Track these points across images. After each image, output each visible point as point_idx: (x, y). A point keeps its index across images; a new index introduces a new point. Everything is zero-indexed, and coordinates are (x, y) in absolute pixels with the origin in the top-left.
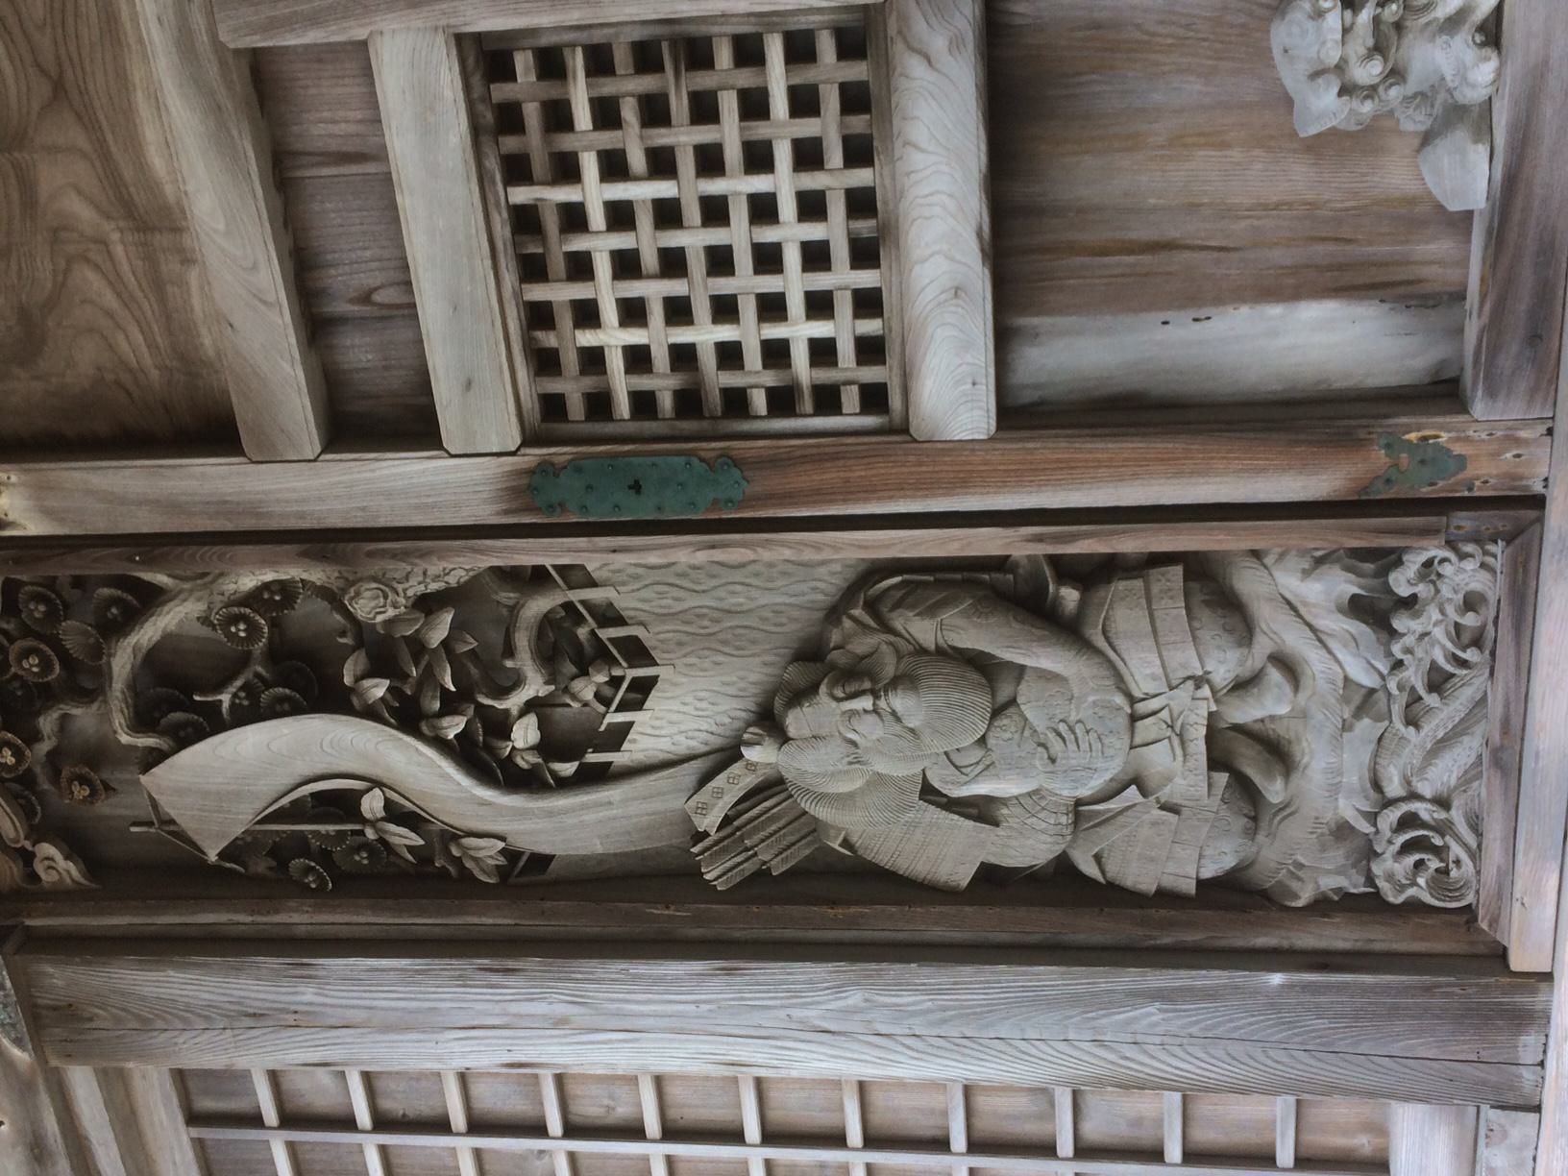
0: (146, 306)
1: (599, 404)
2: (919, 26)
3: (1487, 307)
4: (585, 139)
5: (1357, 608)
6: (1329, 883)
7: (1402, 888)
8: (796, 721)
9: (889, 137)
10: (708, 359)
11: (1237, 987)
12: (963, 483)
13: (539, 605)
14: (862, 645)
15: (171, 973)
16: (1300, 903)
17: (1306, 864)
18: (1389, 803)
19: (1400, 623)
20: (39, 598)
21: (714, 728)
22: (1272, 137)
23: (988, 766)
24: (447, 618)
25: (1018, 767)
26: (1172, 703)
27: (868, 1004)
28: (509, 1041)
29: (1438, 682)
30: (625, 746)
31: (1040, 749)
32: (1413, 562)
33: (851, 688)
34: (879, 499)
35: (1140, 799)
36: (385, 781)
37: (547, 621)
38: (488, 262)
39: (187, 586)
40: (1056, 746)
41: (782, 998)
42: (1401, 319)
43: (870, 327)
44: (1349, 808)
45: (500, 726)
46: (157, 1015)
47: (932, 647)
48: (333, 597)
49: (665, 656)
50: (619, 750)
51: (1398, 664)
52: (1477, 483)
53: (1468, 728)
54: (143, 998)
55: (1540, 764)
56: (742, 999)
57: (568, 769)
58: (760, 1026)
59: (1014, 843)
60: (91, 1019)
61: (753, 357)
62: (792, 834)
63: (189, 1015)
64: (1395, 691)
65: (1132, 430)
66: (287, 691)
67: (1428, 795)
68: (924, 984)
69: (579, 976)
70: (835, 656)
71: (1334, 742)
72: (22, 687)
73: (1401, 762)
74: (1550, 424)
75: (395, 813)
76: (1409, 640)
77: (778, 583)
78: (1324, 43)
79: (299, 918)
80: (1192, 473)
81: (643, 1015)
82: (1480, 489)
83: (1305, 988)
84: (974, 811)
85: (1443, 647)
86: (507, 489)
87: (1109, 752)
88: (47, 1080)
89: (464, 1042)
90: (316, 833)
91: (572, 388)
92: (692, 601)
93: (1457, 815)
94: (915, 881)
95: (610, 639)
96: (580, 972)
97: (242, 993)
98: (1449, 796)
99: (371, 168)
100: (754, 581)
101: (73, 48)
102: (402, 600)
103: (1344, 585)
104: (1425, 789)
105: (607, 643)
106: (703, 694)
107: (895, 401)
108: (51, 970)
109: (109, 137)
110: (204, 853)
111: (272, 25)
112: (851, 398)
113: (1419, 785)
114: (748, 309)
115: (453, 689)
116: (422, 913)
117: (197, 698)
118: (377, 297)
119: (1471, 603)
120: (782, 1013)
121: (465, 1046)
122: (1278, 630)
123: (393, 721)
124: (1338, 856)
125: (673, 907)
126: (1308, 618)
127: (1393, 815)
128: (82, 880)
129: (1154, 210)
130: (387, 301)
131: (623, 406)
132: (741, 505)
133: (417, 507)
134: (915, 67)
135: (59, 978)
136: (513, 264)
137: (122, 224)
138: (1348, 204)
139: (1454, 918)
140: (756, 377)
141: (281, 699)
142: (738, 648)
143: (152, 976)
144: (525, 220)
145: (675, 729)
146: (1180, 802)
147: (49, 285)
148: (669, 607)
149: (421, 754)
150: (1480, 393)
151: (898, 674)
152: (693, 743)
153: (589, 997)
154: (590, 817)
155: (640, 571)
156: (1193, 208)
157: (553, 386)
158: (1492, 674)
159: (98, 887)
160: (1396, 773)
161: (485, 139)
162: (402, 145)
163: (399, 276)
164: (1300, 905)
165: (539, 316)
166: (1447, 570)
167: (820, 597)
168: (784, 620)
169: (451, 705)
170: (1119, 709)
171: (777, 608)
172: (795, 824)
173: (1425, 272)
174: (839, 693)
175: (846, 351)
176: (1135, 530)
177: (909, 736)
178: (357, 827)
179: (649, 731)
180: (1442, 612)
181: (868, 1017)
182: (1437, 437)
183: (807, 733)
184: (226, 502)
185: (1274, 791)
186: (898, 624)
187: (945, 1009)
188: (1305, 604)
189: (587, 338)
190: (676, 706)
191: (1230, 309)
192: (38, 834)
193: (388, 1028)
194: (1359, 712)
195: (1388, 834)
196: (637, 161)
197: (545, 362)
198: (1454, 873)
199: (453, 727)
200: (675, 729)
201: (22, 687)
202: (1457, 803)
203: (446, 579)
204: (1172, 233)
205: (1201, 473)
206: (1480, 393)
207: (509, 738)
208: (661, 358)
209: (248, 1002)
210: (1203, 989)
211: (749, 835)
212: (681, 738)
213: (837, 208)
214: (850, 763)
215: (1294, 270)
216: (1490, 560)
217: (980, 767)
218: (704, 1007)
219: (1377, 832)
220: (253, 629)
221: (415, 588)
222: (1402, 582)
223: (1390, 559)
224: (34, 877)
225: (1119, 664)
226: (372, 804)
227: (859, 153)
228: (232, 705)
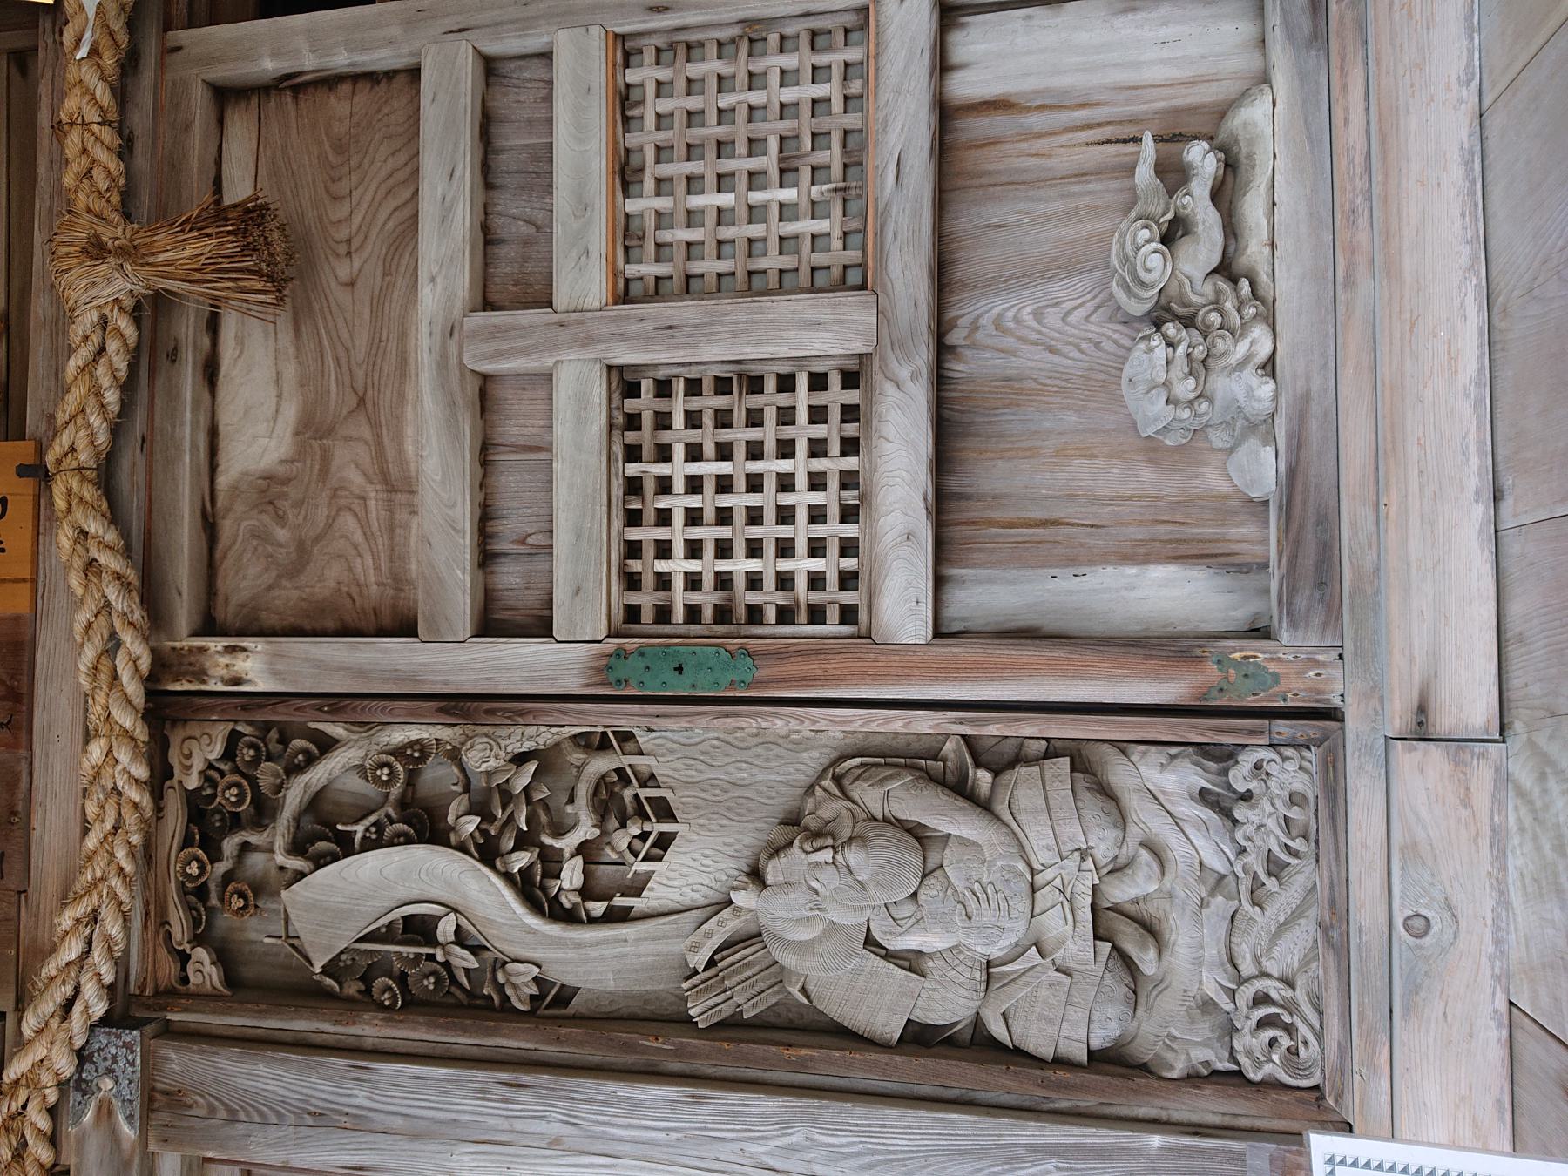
0: (380, 541)
1: (663, 614)
2: (893, 363)
3: (1284, 561)
4: (678, 437)
5: (1204, 796)
6: (1200, 1055)
7: (1258, 1064)
8: (774, 871)
9: (869, 438)
10: (740, 583)
11: (1123, 1148)
12: (906, 676)
13: (602, 764)
14: (827, 812)
15: (261, 1066)
16: (1174, 1075)
17: (1179, 1036)
18: (1242, 980)
19: (1240, 812)
20: (251, 746)
21: (713, 884)
22: (1125, 452)
23: (918, 921)
24: (532, 767)
25: (946, 925)
26: (1063, 872)
27: (808, 1143)
28: (509, 1159)
29: (1275, 867)
30: (645, 893)
31: (960, 906)
32: (1247, 760)
33: (817, 844)
34: (847, 686)
35: (1039, 960)
36: (460, 908)
37: (602, 780)
38: (605, 509)
39: (355, 737)
40: (972, 903)
41: (739, 1131)
42: (1226, 581)
43: (849, 563)
44: (1212, 983)
45: (551, 862)
46: (242, 1107)
47: (880, 817)
48: (455, 756)
49: (685, 816)
50: (639, 896)
51: (1242, 851)
52: (1290, 695)
53: (1303, 912)
54: (235, 1089)
55: (1364, 938)
56: (705, 1129)
57: (598, 908)
58: (718, 1160)
59: (937, 996)
60: (190, 1107)
61: (769, 582)
62: (763, 980)
63: (265, 1109)
64: (1241, 875)
65: (1029, 641)
66: (406, 827)
67: (1276, 974)
68: (857, 1125)
69: (576, 1096)
70: (807, 820)
71: (1195, 917)
72: (220, 820)
73: (1251, 940)
74: (1340, 651)
75: (460, 937)
76: (1249, 829)
77: (773, 764)
78: (1154, 368)
79: (369, 1029)
80: (1073, 677)
81: (622, 1140)
82: (1292, 700)
83: (1181, 1151)
84: (907, 964)
85: (1277, 837)
86: (592, 668)
87: (1014, 914)
88: (142, 1160)
89: (474, 1156)
90: (399, 954)
91: (646, 599)
92: (709, 774)
93: (1301, 996)
94: (857, 1034)
95: (646, 798)
96: (578, 1092)
97: (310, 1092)
98: (1293, 978)
99: (542, 456)
100: (756, 762)
101: (376, 378)
102: (502, 754)
103: (1192, 776)
104: (1272, 967)
105: (644, 801)
106: (708, 852)
107: (863, 616)
108: (173, 1056)
109: (385, 432)
110: (312, 965)
111: (498, 355)
112: (833, 614)
113: (1268, 964)
114: (770, 549)
115: (525, 829)
116: (465, 1031)
117: (339, 827)
118: (530, 541)
119: (1294, 799)
120: (737, 1146)
121: (474, 1160)
122: (1147, 819)
123: (476, 854)
124: (1205, 1029)
125: (661, 1040)
126: (1168, 806)
127: (1247, 992)
128: (218, 985)
129: (1046, 498)
130: (536, 543)
131: (679, 614)
132: (749, 687)
133: (526, 679)
134: (889, 388)
135: (179, 1062)
136: (621, 514)
137: (379, 487)
138: (1181, 498)
139: (1304, 1094)
140: (770, 598)
141: (398, 834)
142: (738, 814)
143: (244, 1068)
144: (633, 486)
145: (682, 882)
146: (1072, 965)
147: (322, 525)
148: (692, 777)
149: (492, 884)
150: (1284, 625)
151: (855, 834)
152: (696, 896)
153: (583, 1119)
154: (608, 951)
155: (675, 746)
156: (1072, 497)
157: (634, 598)
158: (1317, 861)
159: (229, 993)
160: (1247, 950)
161: (616, 433)
162: (562, 433)
163: (546, 526)
164: (1175, 1076)
165: (633, 549)
166: (1273, 769)
167: (802, 777)
168: (774, 794)
169: (522, 842)
170: (1022, 875)
171: (769, 784)
172: (767, 972)
173: (1236, 547)
174: (808, 847)
175: (832, 580)
176: (1031, 719)
177: (858, 887)
178: (431, 951)
179: (665, 881)
180: (1273, 805)
181: (809, 1156)
182: (1256, 657)
183: (781, 879)
184: (396, 670)
185: (1147, 961)
186: (855, 795)
187: (873, 1152)
188: (1164, 793)
189: (662, 566)
190: (686, 860)
191: (1100, 568)
192: (198, 940)
193: (416, 1136)
194: (1213, 892)
195: (1245, 1011)
196: (709, 449)
197: (632, 582)
198: (1302, 1053)
199: (520, 860)
200: (682, 882)
201: (220, 820)
202: (1300, 982)
203: (537, 739)
204: (1057, 514)
205: (1081, 677)
206: (1284, 625)
207: (558, 877)
208: (708, 581)
209: (313, 1101)
210: (1093, 1148)
211: (730, 976)
212: (687, 890)
213: (833, 483)
214: (811, 909)
215: (1143, 542)
216: (1306, 764)
217: (913, 920)
218: (674, 1135)
219: (1237, 1009)
220: (393, 774)
221: (516, 747)
222: (1240, 777)
223: (1224, 756)
224: (185, 980)
225: (1021, 835)
226: (446, 929)
227: (850, 446)
228: (364, 838)
